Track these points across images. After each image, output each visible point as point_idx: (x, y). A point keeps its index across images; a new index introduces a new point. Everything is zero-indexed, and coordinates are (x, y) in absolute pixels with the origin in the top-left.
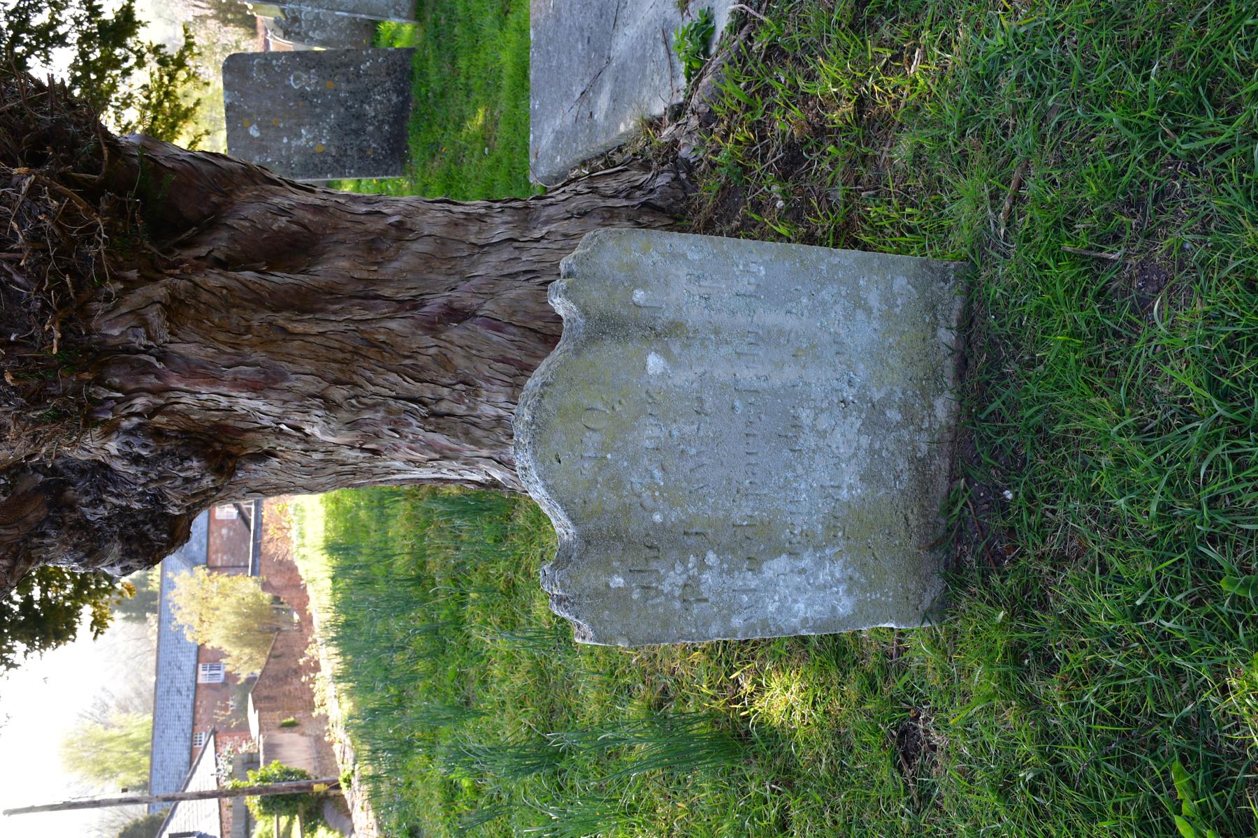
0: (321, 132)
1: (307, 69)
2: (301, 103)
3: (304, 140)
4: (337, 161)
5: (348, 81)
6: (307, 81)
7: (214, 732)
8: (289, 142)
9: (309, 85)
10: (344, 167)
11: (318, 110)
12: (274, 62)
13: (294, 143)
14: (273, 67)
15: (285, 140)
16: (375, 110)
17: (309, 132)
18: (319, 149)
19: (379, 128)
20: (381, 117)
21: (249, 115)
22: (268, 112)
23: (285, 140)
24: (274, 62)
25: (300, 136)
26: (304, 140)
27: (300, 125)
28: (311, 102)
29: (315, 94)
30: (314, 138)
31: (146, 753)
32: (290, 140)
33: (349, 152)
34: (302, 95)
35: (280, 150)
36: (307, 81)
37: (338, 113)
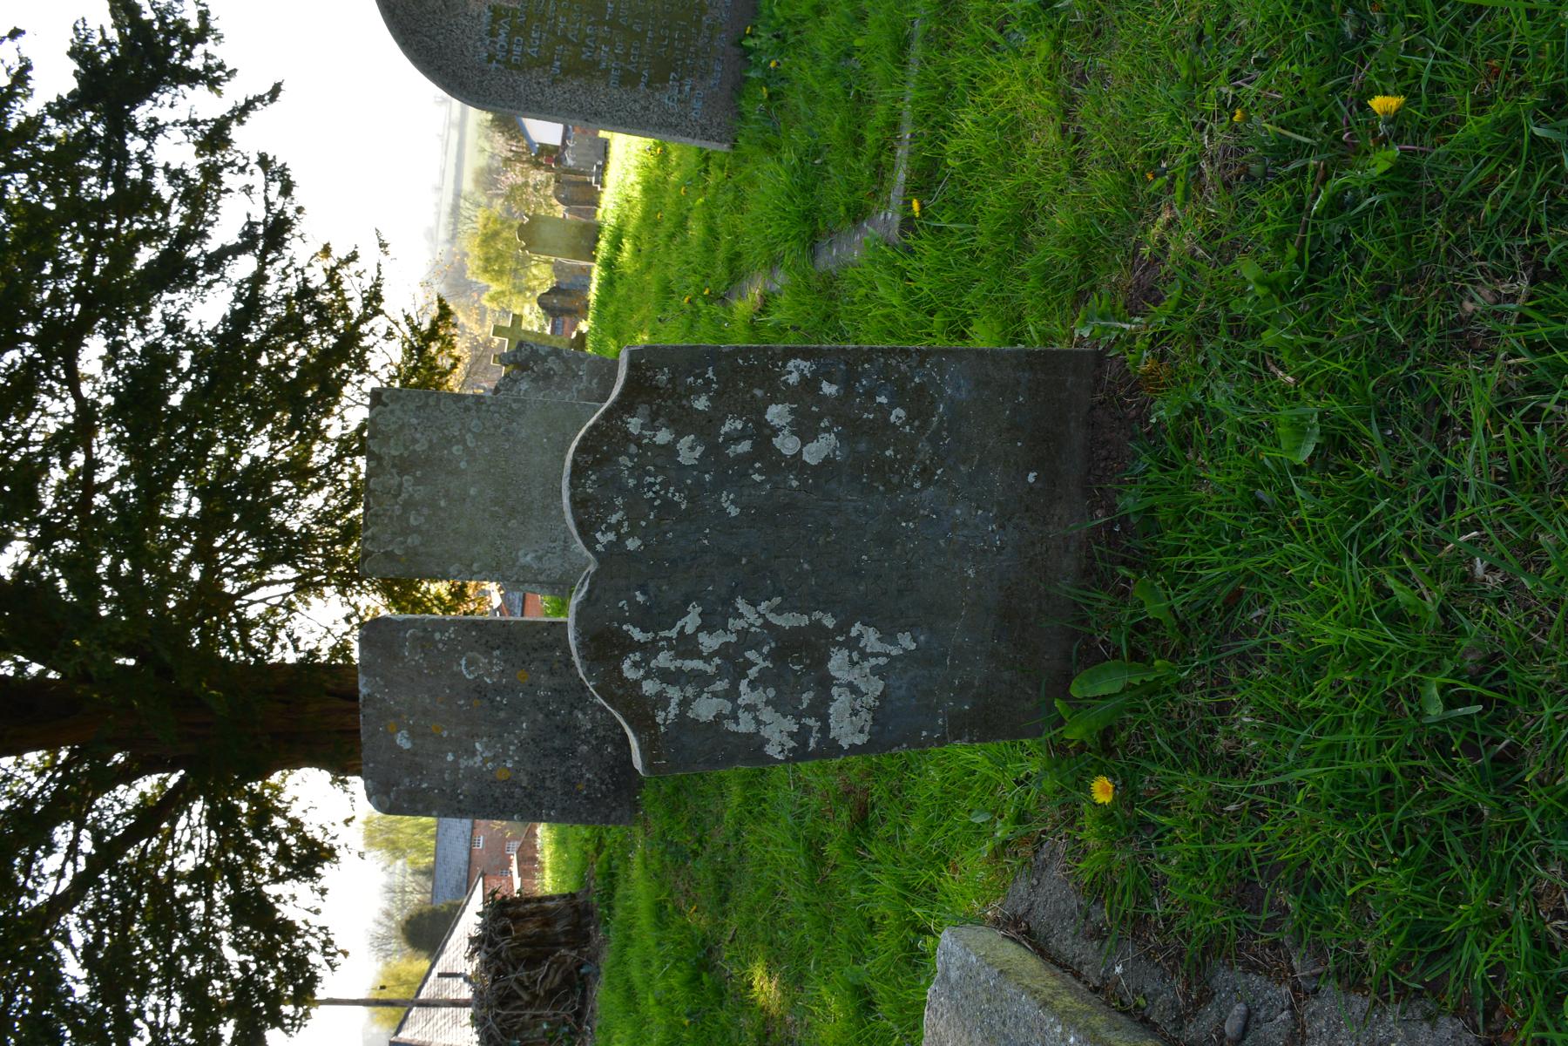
0: (505, 749)
1: (488, 649)
2: (476, 702)
3: (478, 759)
4: (530, 796)
5: (552, 672)
6: (487, 668)
7: (483, 875)
8: (455, 761)
9: (490, 675)
10: (540, 805)
11: (502, 715)
12: (437, 636)
13: (463, 763)
14: (435, 643)
15: (450, 758)
16: (593, 720)
17: (486, 747)
18: (502, 775)
19: (597, 749)
20: (601, 732)
21: (397, 715)
22: (425, 713)
23: (450, 758)
24: (437, 636)
25: (473, 753)
26: (478, 759)
27: (474, 736)
28: (492, 701)
29: (498, 689)
30: (494, 758)
31: (431, 837)
32: (457, 757)
33: (548, 783)
34: (479, 690)
35: (442, 772)
36: (487, 668)
37: (534, 721)
